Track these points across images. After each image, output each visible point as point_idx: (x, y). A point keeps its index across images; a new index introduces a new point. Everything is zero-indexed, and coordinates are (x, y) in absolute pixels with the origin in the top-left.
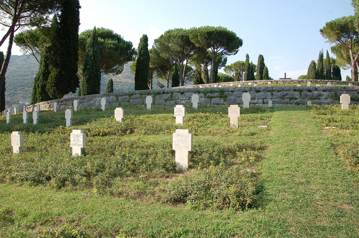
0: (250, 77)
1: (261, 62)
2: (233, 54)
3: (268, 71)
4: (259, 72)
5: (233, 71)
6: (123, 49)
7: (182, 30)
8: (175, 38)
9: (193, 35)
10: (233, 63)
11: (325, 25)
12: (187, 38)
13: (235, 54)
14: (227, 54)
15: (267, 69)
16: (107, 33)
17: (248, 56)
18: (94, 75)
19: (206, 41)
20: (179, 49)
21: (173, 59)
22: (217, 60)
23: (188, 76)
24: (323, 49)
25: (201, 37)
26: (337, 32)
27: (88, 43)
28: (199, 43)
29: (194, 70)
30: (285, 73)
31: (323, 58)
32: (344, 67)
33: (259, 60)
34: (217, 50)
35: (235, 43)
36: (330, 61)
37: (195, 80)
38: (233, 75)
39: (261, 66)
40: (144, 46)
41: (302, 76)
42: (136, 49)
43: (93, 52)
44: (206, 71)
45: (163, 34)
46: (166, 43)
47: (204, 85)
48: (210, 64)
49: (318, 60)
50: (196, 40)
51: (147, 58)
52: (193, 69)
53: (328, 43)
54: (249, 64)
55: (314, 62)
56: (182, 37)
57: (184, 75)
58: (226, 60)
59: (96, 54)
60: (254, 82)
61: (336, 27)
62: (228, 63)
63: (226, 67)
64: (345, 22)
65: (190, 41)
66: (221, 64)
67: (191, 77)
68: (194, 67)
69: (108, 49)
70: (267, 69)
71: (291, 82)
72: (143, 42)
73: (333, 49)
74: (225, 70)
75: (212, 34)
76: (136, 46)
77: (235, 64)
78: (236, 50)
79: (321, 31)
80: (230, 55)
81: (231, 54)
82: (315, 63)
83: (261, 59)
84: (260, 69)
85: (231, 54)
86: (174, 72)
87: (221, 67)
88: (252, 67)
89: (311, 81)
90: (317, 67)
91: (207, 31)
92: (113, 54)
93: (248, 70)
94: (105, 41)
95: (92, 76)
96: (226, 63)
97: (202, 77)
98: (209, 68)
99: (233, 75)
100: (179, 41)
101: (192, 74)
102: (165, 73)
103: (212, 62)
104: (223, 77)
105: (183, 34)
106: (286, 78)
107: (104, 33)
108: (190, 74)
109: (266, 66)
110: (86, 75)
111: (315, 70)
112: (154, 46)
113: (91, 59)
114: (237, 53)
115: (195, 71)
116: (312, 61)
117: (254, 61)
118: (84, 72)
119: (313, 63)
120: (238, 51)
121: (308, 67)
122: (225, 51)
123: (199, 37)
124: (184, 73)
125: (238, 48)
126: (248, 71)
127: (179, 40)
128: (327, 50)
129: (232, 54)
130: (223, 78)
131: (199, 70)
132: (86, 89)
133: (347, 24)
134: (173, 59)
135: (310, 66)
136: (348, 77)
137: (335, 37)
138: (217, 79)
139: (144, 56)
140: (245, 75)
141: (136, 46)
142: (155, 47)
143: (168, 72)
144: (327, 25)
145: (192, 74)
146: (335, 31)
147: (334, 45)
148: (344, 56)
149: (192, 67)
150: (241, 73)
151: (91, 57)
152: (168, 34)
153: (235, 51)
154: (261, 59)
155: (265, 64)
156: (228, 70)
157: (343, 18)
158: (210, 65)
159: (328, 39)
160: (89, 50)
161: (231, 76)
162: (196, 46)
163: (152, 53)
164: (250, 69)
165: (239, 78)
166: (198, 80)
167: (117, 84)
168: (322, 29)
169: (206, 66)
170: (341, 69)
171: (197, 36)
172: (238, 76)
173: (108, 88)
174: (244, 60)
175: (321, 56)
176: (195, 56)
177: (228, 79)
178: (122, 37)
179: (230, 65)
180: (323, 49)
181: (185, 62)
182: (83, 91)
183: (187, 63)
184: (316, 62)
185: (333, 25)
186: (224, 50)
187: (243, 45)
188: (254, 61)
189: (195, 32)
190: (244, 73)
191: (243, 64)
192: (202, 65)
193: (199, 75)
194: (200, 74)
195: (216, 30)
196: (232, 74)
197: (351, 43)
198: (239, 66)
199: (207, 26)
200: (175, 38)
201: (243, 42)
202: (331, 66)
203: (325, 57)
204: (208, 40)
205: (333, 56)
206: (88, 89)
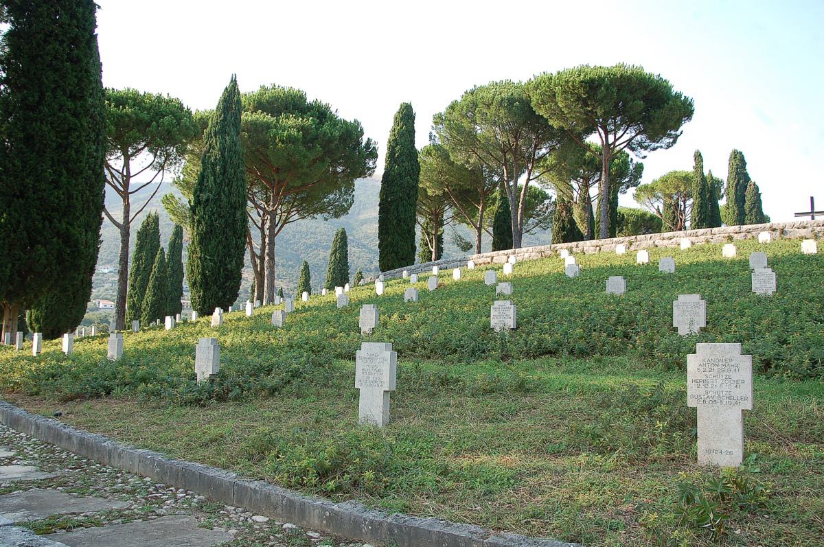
0: (709, 217)
1: (737, 169)
2: (663, 145)
3: (760, 194)
4: (732, 196)
5: (658, 198)
6: (330, 141)
7: (509, 83)
8: (488, 106)
9: (541, 94)
12: (526, 104)
13: (668, 147)
14: (646, 148)
16: (287, 97)
17: (698, 157)
18: (223, 220)
19: (581, 107)
20: (502, 139)
21: (492, 171)
22: (614, 169)
23: (538, 215)
25: (566, 99)
27: (210, 126)
28: (561, 116)
29: (553, 200)
30: (812, 198)
33: (731, 165)
34: (615, 137)
35: (671, 109)
37: (556, 225)
39: (739, 181)
40: (401, 135)
42: (373, 141)
43: (222, 150)
44: (587, 201)
45: (459, 100)
46: (465, 123)
47: (577, 246)
48: (597, 181)
50: (550, 108)
51: (413, 169)
52: (551, 198)
54: (704, 179)
56: (511, 101)
57: (521, 214)
58: (639, 168)
59: (231, 158)
62: (646, 179)
63: (641, 190)
66: (627, 180)
67: (545, 219)
68: (552, 190)
69: (283, 142)
70: (757, 188)
72: (401, 125)
74: (637, 197)
75: (599, 86)
76: (378, 133)
77: (664, 180)
78: (673, 132)
80: (654, 149)
83: (738, 162)
84: (736, 191)
86: (499, 208)
87: (628, 187)
88: (713, 185)
91: (582, 77)
92: (297, 157)
93: (701, 194)
94: (278, 121)
95: (217, 224)
96: (641, 177)
97: (576, 217)
98: (594, 191)
100: (501, 115)
101: (549, 210)
102: (472, 213)
103: (601, 176)
105: (512, 94)
106: (816, 210)
107: (277, 98)
108: (544, 210)
109: (753, 180)
110: (199, 222)
112: (434, 133)
113: (214, 171)
114: (674, 142)
115: (554, 203)
117: (719, 169)
118: (194, 212)
120: (677, 136)
122: (639, 138)
123: (559, 99)
124: (520, 206)
125: (676, 126)
127: (502, 112)
129: (661, 147)
130: (632, 219)
131: (565, 199)
132: (198, 266)
134: (492, 171)
138: (616, 223)
139: (403, 162)
141: (378, 133)
142: (437, 135)
143: (480, 208)
145: (549, 210)
149: (546, 190)
150: (682, 203)
151: (214, 165)
152: (470, 98)
153: (669, 136)
154: (738, 162)
155: (750, 176)
156: (644, 198)
158: (597, 184)
160: (210, 145)
161: (653, 211)
162: (552, 127)
163: (431, 156)
164: (708, 190)
165: (675, 217)
166: (564, 225)
169: (586, 186)
171: (554, 95)
172: (674, 212)
173: (335, 252)
174: (688, 167)
176: (551, 160)
178: (333, 109)
181: (522, 181)
182: (192, 271)
183: (529, 180)
187: (694, 116)
188: (719, 169)
189: (548, 87)
190: (690, 202)
191: (686, 179)
192: (574, 184)
193: (567, 213)
194: (569, 210)
195: (609, 73)
196: (653, 207)
198: (677, 185)
199: (582, 66)
200: (488, 106)
201: (696, 106)
204: (587, 105)
206: (203, 266)
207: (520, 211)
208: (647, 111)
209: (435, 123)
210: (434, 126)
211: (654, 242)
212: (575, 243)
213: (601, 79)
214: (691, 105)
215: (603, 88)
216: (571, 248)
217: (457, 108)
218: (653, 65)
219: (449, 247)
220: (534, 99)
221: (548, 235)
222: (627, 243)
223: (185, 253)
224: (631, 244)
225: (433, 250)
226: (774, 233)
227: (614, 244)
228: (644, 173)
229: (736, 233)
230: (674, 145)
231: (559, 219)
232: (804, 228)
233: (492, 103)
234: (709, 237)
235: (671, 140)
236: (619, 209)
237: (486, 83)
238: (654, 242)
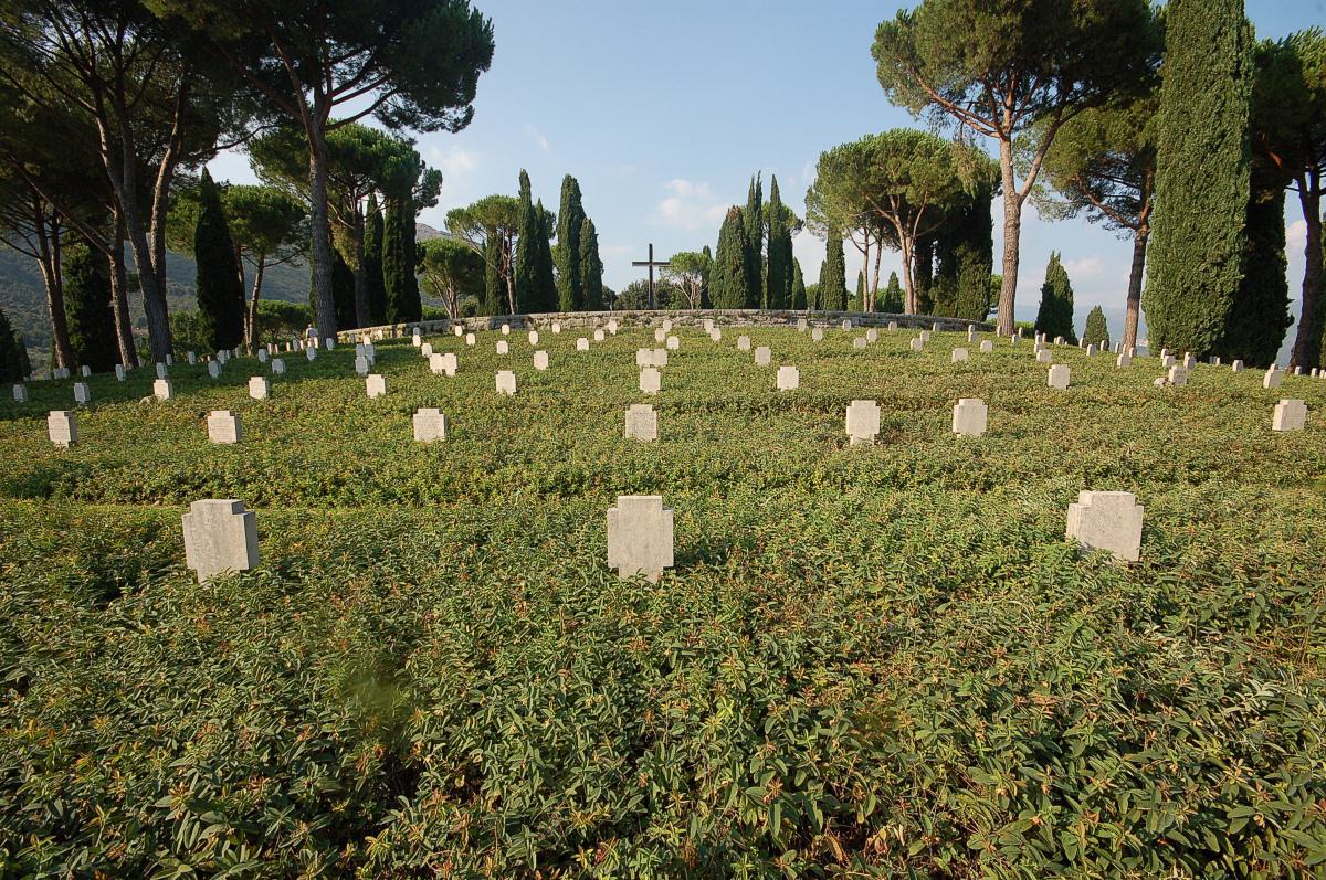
1: (570, 200)
2: (447, 123)
4: (565, 236)
10: (475, 202)
17: (525, 179)
30: (651, 246)
38: (483, 244)
41: (681, 255)
54: (531, 209)
58: (435, 179)
83: (572, 190)
84: (570, 228)
88: (542, 217)
93: (529, 228)
96: (439, 194)
99: (483, 244)
104: (449, 249)
106: (654, 260)
135: (725, 224)
140: (518, 245)
150: (507, 238)
154: (572, 190)
155: (585, 211)
172: (498, 250)
174: (512, 191)
175: (756, 195)
177: (465, 256)
179: (466, 209)
188: (549, 199)
190: (515, 239)
191: (510, 207)
203: (766, 198)
228: (444, 187)
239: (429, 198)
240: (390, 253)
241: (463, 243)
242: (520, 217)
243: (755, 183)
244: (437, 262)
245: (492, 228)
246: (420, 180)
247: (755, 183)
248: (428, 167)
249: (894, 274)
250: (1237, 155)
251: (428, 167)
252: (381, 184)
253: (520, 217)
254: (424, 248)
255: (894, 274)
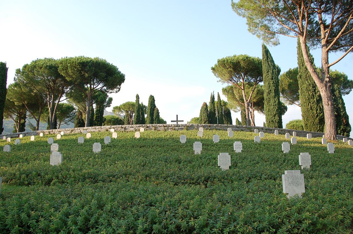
0: (141, 121)
1: (151, 102)
2: (114, 91)
3: (159, 113)
4: (149, 113)
8: (41, 68)
10: (122, 104)
11: (217, 63)
13: (117, 92)
15: (158, 110)
17: (138, 97)
24: (214, 91)
26: (229, 69)
28: (71, 77)
30: (177, 115)
31: (215, 100)
32: (235, 110)
36: (221, 103)
37: (76, 121)
39: (151, 107)
41: (195, 118)
47: (52, 131)
49: (210, 102)
53: (220, 83)
55: (206, 103)
58: (111, 100)
60: (122, 128)
61: (228, 65)
64: (237, 61)
65: (59, 74)
71: (177, 128)
73: (225, 91)
75: (87, 65)
79: (213, 69)
80: (111, 93)
81: (112, 92)
82: (207, 106)
83: (152, 100)
84: (150, 111)
85: (112, 92)
89: (204, 127)
90: (208, 110)
93: (138, 111)
96: (111, 103)
104: (112, 119)
106: (176, 120)
109: (157, 107)
111: (207, 112)
112: (16, 78)
114: (119, 90)
116: (204, 103)
119: (205, 104)
121: (200, 109)
126: (138, 113)
127: (46, 71)
128: (218, 93)
129: (114, 92)
133: (239, 62)
135: (202, 108)
136: (237, 120)
137: (227, 75)
140: (135, 116)
144: (218, 62)
146: (228, 69)
147: (226, 85)
148: (237, 97)
154: (152, 100)
155: (156, 105)
157: (235, 56)
159: (219, 79)
162: (67, 80)
164: (141, 109)
167: (7, 124)
168: (213, 67)
170: (232, 112)
174: (133, 100)
175: (213, 98)
177: (118, 121)
180: (214, 91)
184: (208, 104)
185: (226, 62)
186: (103, 87)
188: (145, 102)
189: (67, 63)
191: (133, 105)
197: (243, 83)
198: (128, 107)
199: (82, 57)
202: (222, 109)
203: (216, 99)
205: (224, 98)
207: (54, 114)
208: (106, 77)
209: (16, 73)
210: (16, 74)
211: (80, 131)
212: (52, 130)
213: (88, 62)
214: (124, 77)
215: (88, 67)
216: (50, 132)
217: (27, 68)
218: (111, 60)
219: (27, 128)
220: (60, 67)
221: (74, 125)
222: (71, 131)
223: (50, 119)
224: (72, 131)
225: (18, 130)
226: (122, 129)
227: (66, 131)
228: (113, 102)
229: (109, 128)
230: (119, 92)
231: (78, 119)
232: (132, 127)
233: (42, 67)
234: (100, 129)
235: (118, 90)
236: (104, 116)
237: (43, 58)
238: (80, 131)
239: (109, 104)
240: (96, 120)
241: (117, 116)
242: (135, 108)
243: (212, 95)
244: (109, 123)
245: (127, 112)
246: (107, 99)
247: (212, 95)
248: (109, 97)
249: (264, 122)
250: (274, 94)
251: (109, 97)
252: (97, 102)
253: (135, 108)
254: (105, 118)
255: (264, 122)
